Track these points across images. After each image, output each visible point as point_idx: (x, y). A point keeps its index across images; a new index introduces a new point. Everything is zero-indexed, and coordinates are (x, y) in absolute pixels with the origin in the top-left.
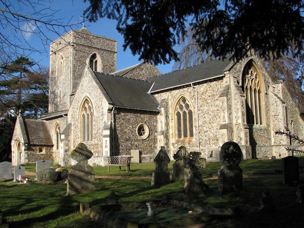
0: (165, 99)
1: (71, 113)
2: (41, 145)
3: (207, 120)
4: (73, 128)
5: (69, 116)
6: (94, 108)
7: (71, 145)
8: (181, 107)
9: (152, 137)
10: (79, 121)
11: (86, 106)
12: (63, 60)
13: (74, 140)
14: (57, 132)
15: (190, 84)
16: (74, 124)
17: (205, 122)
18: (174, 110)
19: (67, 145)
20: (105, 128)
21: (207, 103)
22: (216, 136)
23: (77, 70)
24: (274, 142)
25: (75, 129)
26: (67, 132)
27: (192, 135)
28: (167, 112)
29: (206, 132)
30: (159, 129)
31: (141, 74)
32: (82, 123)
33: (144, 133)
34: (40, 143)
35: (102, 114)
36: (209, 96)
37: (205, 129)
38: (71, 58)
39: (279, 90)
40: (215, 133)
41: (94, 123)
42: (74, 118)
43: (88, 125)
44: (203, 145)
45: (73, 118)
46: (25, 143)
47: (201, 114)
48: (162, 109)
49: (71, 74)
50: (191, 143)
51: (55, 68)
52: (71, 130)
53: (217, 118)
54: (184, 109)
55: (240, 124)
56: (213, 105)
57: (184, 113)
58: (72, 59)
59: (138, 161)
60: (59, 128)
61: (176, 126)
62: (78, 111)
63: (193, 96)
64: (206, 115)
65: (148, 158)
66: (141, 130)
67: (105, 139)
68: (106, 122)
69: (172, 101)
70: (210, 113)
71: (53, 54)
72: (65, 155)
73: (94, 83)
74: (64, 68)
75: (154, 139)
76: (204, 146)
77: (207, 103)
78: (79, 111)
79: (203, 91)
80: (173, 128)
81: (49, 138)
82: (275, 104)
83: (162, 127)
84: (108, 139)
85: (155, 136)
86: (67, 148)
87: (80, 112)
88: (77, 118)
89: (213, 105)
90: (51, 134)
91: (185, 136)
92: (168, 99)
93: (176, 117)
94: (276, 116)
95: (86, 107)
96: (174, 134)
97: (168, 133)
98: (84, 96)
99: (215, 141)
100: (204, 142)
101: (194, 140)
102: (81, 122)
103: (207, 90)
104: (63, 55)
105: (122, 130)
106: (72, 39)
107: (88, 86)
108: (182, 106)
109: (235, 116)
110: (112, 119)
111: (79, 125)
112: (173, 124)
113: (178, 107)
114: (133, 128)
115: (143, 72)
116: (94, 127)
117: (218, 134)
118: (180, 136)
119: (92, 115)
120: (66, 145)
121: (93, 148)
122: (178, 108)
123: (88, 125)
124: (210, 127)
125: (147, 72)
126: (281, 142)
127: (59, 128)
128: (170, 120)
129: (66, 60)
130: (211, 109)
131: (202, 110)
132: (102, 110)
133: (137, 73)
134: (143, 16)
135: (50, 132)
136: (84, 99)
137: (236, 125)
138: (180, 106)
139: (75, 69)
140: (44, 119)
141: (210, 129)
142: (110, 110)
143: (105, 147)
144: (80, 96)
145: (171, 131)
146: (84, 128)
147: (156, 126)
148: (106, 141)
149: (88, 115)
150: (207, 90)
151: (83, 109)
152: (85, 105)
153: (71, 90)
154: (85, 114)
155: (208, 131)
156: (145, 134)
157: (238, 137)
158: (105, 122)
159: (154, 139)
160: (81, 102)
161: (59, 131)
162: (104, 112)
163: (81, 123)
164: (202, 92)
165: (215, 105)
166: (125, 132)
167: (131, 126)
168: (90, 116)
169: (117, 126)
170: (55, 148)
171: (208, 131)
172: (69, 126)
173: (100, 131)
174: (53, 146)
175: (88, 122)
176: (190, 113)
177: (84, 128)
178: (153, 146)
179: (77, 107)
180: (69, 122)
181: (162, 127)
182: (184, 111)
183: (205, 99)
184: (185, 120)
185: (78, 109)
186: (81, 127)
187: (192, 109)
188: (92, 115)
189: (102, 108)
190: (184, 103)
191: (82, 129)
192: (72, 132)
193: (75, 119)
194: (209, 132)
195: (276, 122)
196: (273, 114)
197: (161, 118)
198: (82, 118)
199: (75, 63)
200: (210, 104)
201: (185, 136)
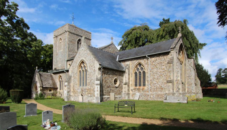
0: (128, 64)
1: (71, 70)
2: (51, 88)
3: (156, 77)
4: (72, 78)
5: (70, 71)
6: (88, 67)
7: (71, 88)
8: (138, 69)
9: (120, 86)
10: (77, 74)
11: (82, 65)
12: (61, 41)
13: (74, 86)
14: (60, 80)
15: (146, 56)
16: (73, 76)
17: (154, 78)
18: (133, 71)
19: (69, 88)
20: (97, 80)
21: (156, 67)
22: (161, 87)
23: (70, 47)
24: (187, 91)
25: (74, 79)
26: (69, 81)
27: (144, 85)
28: (129, 71)
29: (154, 84)
30: (124, 81)
31: (109, 50)
32: (79, 76)
33: (117, 83)
34: (50, 87)
35: (94, 71)
36: (158, 63)
37: (154, 82)
38: (67, 40)
39: (191, 63)
40: (161, 85)
41: (88, 76)
42: (74, 73)
43: (83, 77)
44: (152, 92)
45: (72, 72)
46: (40, 87)
47: (152, 74)
48: (127, 70)
49: (67, 49)
50: (144, 90)
51: (57, 45)
52: (71, 80)
53: (162, 77)
54: (140, 70)
55: (179, 80)
56: (160, 69)
57: (140, 72)
58: (67, 40)
59: (114, 99)
60: (61, 79)
61: (134, 80)
62: (77, 68)
63: (147, 63)
64: (155, 74)
65: (118, 98)
66: (116, 81)
67: (96, 86)
68: (97, 75)
69: (132, 65)
70: (158, 73)
71: (55, 37)
72: (67, 94)
73: (89, 52)
74: (63, 46)
75: (122, 87)
76: (153, 92)
77: (156, 67)
78: (77, 68)
79: (154, 60)
80: (132, 81)
81: (54, 84)
82: (189, 70)
83: (126, 80)
84: (99, 86)
85: (122, 85)
86: (69, 90)
87: (78, 69)
88: (76, 73)
89: (160, 69)
90: (56, 82)
91: (83, 85)
92: (130, 64)
93: (134, 75)
94: (189, 77)
95: (82, 66)
96: (132, 85)
97: (129, 83)
98: (81, 59)
99: (161, 90)
100: (153, 90)
101: (146, 88)
102: (78, 75)
103: (157, 60)
104: (61, 38)
105: (106, 81)
106: (67, 29)
107: (84, 53)
108: (139, 68)
109: (176, 75)
110: (100, 74)
111: (77, 77)
112: (132, 78)
113: (136, 69)
114: (111, 80)
115: (110, 49)
116: (88, 78)
117: (163, 85)
118: (136, 85)
119: (86, 72)
120: (68, 89)
121: (87, 91)
122: (136, 70)
123: (83, 77)
124: (158, 81)
125: (112, 50)
126: (192, 91)
127: (61, 79)
128: (131, 76)
129: (63, 41)
130: (159, 71)
131: (152, 71)
132: (94, 68)
133: (107, 49)
134: (32, 65)
135: (56, 80)
136: (81, 61)
137: (176, 81)
138: (137, 69)
139: (69, 46)
140: (52, 73)
141: (157, 82)
142: (100, 69)
143: (97, 91)
144: (77, 60)
145: (131, 83)
146: (81, 79)
147: (122, 79)
148: (97, 87)
149: (83, 71)
150: (157, 60)
151: (80, 67)
152: (81, 65)
153: (67, 58)
154: (81, 71)
155: (156, 84)
156: (117, 84)
157: (177, 88)
158: (96, 75)
159: (122, 87)
160: (78, 63)
161: (61, 80)
162: (96, 70)
163: (78, 76)
164: (153, 61)
165: (162, 69)
166: (107, 82)
167: (110, 79)
168: (85, 72)
169: (103, 78)
170: (58, 90)
171: (156, 84)
172: (70, 78)
173: (93, 81)
174: (57, 88)
175: (83, 75)
176: (144, 73)
177: (81, 79)
178: (121, 90)
179: (75, 66)
180: (70, 75)
181: (126, 80)
182: (138, 71)
183: (155, 65)
184: (140, 77)
185: (77, 68)
186: (78, 78)
187: (146, 71)
188: (86, 72)
189: (94, 67)
190: (140, 67)
191: (79, 79)
192: (72, 81)
193: (74, 73)
194: (156, 84)
195: (189, 80)
196: (188, 75)
197: (126, 75)
198: (79, 73)
199: (69, 43)
200: (158, 68)
201: (140, 85)
